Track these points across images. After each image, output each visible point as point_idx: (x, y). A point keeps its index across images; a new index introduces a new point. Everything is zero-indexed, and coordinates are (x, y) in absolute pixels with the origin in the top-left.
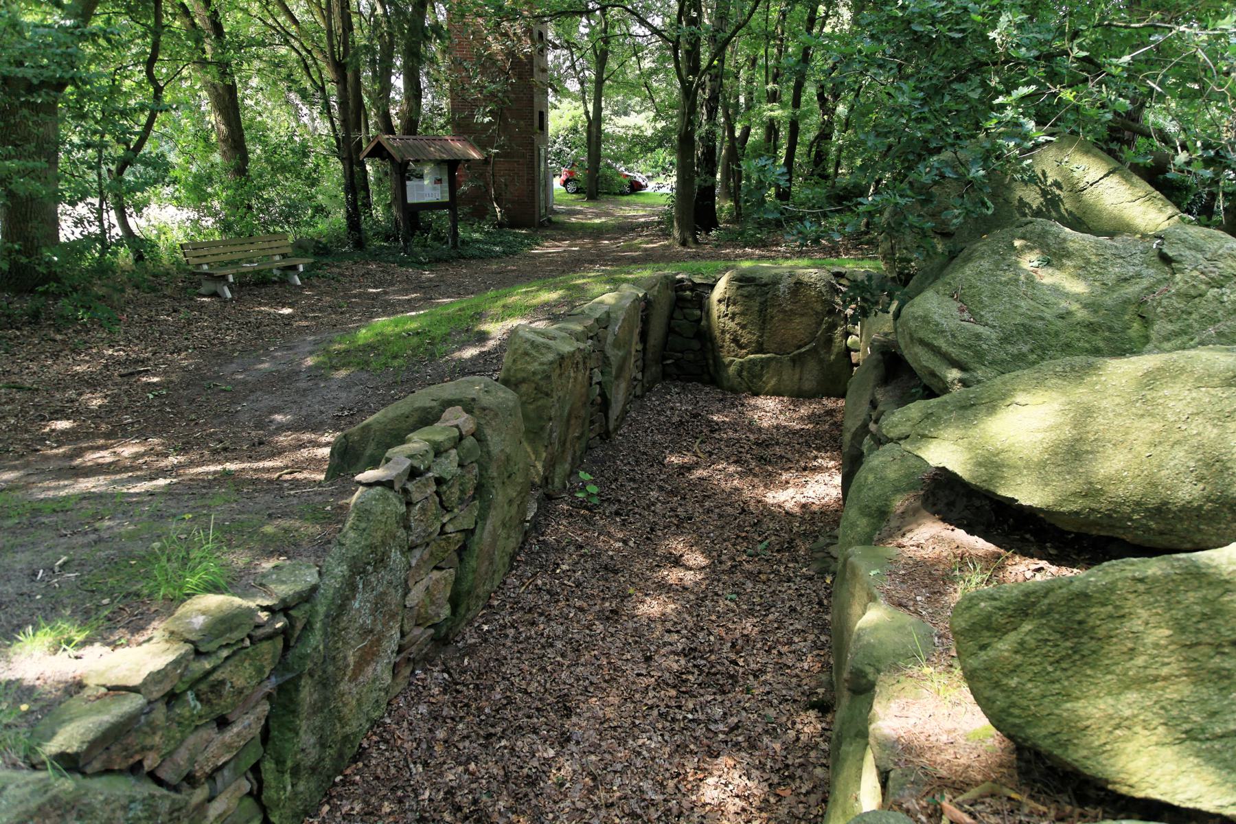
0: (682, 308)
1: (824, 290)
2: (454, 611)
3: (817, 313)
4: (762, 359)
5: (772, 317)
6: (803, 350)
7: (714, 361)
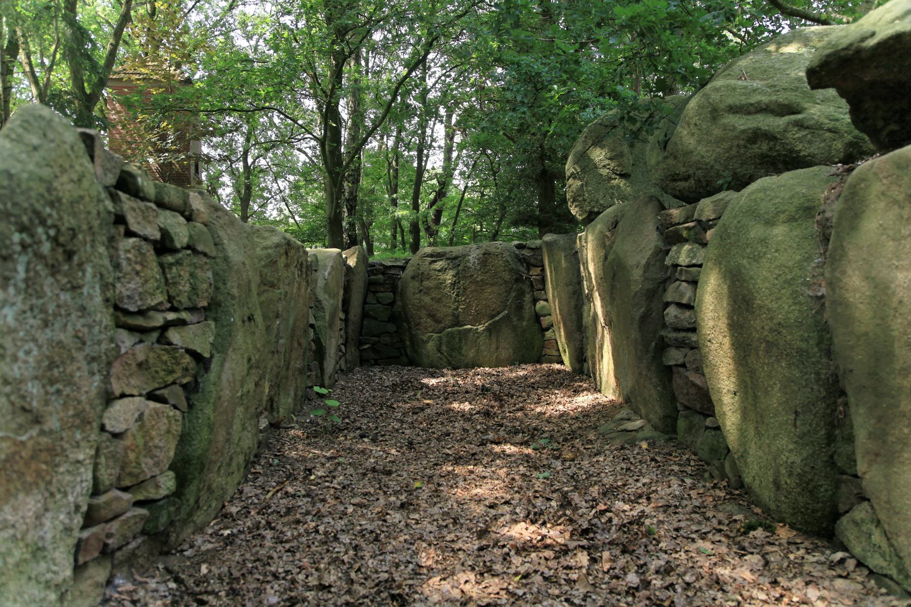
0: (375, 292)
1: (509, 259)
2: (182, 481)
3: (506, 282)
6: (497, 318)
7: (412, 341)
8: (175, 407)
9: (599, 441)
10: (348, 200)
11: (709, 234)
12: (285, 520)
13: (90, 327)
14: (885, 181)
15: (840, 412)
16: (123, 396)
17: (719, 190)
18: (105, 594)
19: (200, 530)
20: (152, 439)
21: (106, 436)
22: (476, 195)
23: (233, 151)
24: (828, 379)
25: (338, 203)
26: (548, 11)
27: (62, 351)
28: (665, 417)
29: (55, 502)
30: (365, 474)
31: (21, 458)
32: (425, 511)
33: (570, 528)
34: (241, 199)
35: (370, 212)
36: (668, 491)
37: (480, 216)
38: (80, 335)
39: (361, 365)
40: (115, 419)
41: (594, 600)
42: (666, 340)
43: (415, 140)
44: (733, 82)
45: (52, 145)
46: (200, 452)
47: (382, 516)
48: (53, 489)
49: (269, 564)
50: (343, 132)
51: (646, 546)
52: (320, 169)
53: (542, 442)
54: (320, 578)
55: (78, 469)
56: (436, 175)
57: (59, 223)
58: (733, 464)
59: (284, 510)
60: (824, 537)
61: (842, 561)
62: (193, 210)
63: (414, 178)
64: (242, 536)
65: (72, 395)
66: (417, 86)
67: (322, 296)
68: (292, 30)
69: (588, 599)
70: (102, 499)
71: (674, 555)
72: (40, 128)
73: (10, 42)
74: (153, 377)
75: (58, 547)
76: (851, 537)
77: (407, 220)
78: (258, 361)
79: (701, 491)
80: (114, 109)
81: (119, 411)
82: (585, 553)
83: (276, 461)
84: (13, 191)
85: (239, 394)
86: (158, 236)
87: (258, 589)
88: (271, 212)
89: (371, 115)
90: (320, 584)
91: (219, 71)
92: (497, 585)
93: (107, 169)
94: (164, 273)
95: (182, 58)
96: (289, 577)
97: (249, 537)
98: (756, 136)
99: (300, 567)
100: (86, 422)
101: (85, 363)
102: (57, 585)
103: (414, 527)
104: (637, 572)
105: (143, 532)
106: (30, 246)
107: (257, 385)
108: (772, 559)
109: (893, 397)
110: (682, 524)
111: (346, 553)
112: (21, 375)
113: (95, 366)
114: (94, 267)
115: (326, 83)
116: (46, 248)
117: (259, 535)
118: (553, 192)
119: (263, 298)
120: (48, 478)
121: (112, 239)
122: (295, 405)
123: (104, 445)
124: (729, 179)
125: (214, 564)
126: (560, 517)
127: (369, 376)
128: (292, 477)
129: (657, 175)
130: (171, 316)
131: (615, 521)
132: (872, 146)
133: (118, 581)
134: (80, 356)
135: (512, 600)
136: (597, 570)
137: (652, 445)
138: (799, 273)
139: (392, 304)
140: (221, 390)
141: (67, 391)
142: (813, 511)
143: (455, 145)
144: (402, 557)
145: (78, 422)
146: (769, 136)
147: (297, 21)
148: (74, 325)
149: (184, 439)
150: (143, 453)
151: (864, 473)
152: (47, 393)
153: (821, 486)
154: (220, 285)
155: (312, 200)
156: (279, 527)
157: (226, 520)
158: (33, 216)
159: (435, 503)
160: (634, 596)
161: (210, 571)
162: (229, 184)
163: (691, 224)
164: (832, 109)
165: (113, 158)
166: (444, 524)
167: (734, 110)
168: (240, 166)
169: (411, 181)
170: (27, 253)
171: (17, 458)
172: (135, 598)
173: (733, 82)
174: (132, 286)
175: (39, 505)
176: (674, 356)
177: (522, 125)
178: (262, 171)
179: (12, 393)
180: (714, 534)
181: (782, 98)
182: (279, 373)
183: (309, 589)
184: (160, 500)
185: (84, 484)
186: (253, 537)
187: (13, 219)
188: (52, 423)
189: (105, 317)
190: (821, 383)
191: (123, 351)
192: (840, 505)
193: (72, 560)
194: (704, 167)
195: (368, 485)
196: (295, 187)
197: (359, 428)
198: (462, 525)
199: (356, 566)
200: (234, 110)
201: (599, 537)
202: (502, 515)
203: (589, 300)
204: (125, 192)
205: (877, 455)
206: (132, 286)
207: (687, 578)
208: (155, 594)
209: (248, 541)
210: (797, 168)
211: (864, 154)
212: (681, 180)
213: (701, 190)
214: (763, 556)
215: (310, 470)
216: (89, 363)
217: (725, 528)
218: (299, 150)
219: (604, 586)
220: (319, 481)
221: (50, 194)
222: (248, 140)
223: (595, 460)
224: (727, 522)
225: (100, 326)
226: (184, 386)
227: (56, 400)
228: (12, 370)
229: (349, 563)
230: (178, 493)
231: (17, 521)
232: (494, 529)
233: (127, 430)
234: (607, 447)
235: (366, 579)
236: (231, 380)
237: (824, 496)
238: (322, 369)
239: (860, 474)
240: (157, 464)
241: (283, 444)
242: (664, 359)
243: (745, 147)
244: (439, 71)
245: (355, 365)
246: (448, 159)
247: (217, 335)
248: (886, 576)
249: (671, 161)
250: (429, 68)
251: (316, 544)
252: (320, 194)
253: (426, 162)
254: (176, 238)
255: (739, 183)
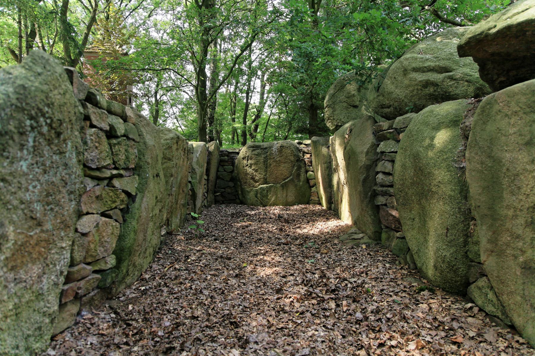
0: (223, 166)
2: (119, 261)
4: (267, 187)
5: (270, 165)
6: (287, 180)
7: (242, 192)
8: (116, 221)
9: (340, 244)
10: (209, 119)
11: (401, 136)
12: (174, 282)
13: (70, 175)
14: (501, 104)
15: (472, 229)
16: (88, 213)
17: (407, 112)
18: (76, 320)
19: (129, 287)
20: (103, 237)
21: (78, 235)
22: (276, 117)
23: (149, 92)
24: (465, 211)
25: (204, 120)
26: (316, 20)
27: (54, 187)
28: (375, 232)
29: (49, 269)
30: (217, 259)
31: (30, 244)
32: (249, 279)
33: (325, 289)
34: (153, 117)
35: (221, 125)
36: (377, 270)
37: (279, 127)
38: (64, 179)
39: (215, 204)
40: (83, 226)
41: (339, 326)
42: (377, 191)
43: (246, 88)
44: (416, 55)
45: (49, 73)
46: (129, 245)
47: (226, 281)
48: (49, 262)
49: (165, 305)
50: (207, 83)
51: (366, 299)
52: (195, 101)
53: (310, 244)
54: (192, 313)
55: (62, 252)
56: (255, 106)
57: (53, 116)
58: (412, 256)
59: (174, 277)
60: (461, 295)
61: (471, 308)
62: (127, 116)
63: (244, 107)
64: (151, 290)
65: (59, 211)
66: (246, 59)
67: (195, 166)
68: (181, 28)
69: (336, 326)
70: (76, 268)
71: (380, 304)
72: (42, 63)
73: (31, 31)
74: (104, 204)
75: (51, 294)
76: (476, 296)
77: (240, 129)
78: (161, 198)
79: (394, 271)
80: (87, 67)
81: (86, 221)
82: (334, 301)
83: (170, 252)
84: (26, 97)
85: (151, 215)
86: (108, 128)
87: (159, 318)
88: (169, 124)
89: (222, 75)
90: (193, 316)
91: (142, 49)
92: (287, 318)
93: (80, 90)
94: (111, 148)
95: (122, 42)
96: (176, 312)
97: (155, 291)
98: (427, 84)
99: (182, 307)
100: (67, 226)
101: (67, 194)
102: (49, 314)
103: (243, 287)
104: (361, 312)
105: (98, 287)
106: (36, 128)
107: (160, 211)
108: (433, 307)
109: (502, 221)
110: (385, 287)
111: (207, 300)
112: (30, 199)
113: (72, 196)
114: (72, 142)
115: (199, 56)
116: (45, 129)
117: (160, 290)
118: (317, 116)
119: (164, 166)
120: (45, 256)
121: (82, 128)
122: (180, 223)
123: (77, 239)
124: (412, 107)
125: (136, 305)
126: (320, 283)
127: (219, 209)
128: (178, 260)
129: (374, 105)
130: (115, 172)
131: (349, 285)
132: (489, 90)
133: (84, 313)
134: (64, 191)
135: (295, 326)
136: (340, 311)
137: (368, 246)
138: (451, 155)
139: (232, 172)
140: (141, 213)
141: (57, 209)
142: (455, 282)
143: (266, 91)
144: (236, 302)
145: (62, 226)
146: (434, 84)
147: (184, 23)
148: (61, 174)
149: (121, 238)
150: (99, 244)
151: (485, 261)
152: (45, 210)
153: (460, 268)
154: (142, 157)
155: (190, 118)
156: (171, 286)
157: (143, 282)
158: (38, 112)
159: (254, 275)
160: (360, 325)
161: (134, 308)
162: (147, 109)
163: (391, 131)
164: (468, 69)
165: (83, 84)
166: (259, 285)
167: (415, 70)
168: (153, 100)
169: (243, 109)
170: (34, 132)
171: (28, 244)
172: (93, 322)
173: (416, 55)
174: (93, 154)
175: (40, 270)
176: (381, 200)
177: (301, 80)
178: (164, 103)
179: (26, 208)
180: (402, 293)
181: (442, 64)
182: (172, 206)
183: (187, 318)
184: (107, 270)
185: (66, 260)
186: (157, 291)
187: (26, 112)
188: (48, 226)
189: (78, 170)
190: (461, 213)
191: (88, 189)
192: (470, 279)
193: (58, 301)
194: (399, 100)
195: (219, 265)
196: (182, 111)
197: (214, 236)
198: (268, 286)
199: (212, 307)
200: (150, 70)
201: (340, 293)
202: (289, 281)
203: (335, 171)
204: (90, 103)
205: (492, 252)
206: (93, 154)
207: (388, 316)
208: (104, 320)
209: (154, 293)
210: (449, 100)
211: (484, 94)
212: (386, 108)
213: (397, 113)
214: (428, 305)
215: (188, 257)
216: (69, 195)
217: (408, 290)
218: (184, 91)
219: (343, 319)
220: (193, 262)
221: (48, 100)
222: (157, 86)
223: (338, 253)
224: (409, 287)
225: (75, 174)
226: (121, 210)
227: (50, 214)
228: (25, 196)
229: (208, 305)
230: (117, 267)
231: (27, 279)
232: (285, 288)
233: (90, 232)
234: (344, 247)
235: (217, 313)
236: (147, 207)
237: (461, 274)
238: (195, 205)
239: (482, 262)
240: (106, 251)
241: (174, 243)
242: (375, 202)
243: (421, 90)
244: (258, 52)
245: (212, 203)
246: (262, 98)
247: (140, 183)
248: (495, 316)
249: (381, 98)
250: (253, 50)
251: (191, 295)
252: (195, 115)
253: (250, 99)
254: (118, 130)
255: (417, 109)
